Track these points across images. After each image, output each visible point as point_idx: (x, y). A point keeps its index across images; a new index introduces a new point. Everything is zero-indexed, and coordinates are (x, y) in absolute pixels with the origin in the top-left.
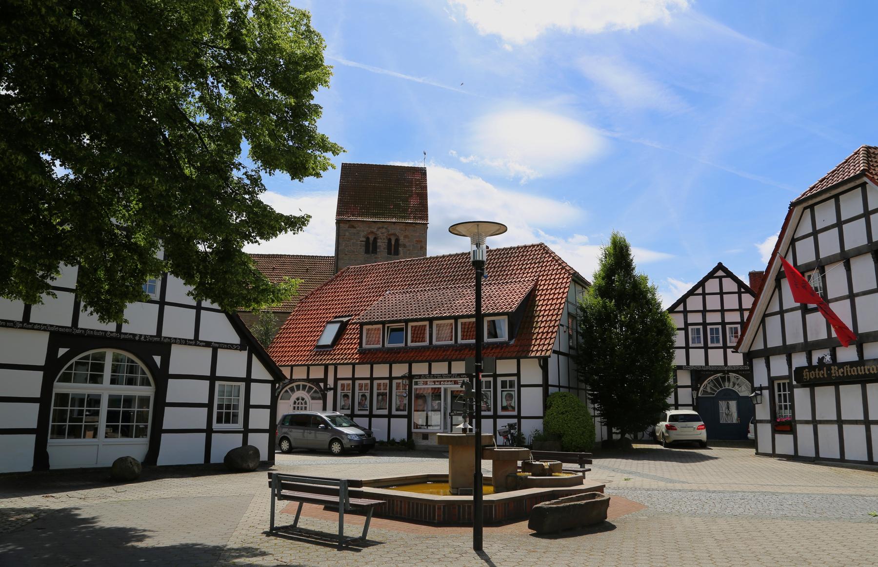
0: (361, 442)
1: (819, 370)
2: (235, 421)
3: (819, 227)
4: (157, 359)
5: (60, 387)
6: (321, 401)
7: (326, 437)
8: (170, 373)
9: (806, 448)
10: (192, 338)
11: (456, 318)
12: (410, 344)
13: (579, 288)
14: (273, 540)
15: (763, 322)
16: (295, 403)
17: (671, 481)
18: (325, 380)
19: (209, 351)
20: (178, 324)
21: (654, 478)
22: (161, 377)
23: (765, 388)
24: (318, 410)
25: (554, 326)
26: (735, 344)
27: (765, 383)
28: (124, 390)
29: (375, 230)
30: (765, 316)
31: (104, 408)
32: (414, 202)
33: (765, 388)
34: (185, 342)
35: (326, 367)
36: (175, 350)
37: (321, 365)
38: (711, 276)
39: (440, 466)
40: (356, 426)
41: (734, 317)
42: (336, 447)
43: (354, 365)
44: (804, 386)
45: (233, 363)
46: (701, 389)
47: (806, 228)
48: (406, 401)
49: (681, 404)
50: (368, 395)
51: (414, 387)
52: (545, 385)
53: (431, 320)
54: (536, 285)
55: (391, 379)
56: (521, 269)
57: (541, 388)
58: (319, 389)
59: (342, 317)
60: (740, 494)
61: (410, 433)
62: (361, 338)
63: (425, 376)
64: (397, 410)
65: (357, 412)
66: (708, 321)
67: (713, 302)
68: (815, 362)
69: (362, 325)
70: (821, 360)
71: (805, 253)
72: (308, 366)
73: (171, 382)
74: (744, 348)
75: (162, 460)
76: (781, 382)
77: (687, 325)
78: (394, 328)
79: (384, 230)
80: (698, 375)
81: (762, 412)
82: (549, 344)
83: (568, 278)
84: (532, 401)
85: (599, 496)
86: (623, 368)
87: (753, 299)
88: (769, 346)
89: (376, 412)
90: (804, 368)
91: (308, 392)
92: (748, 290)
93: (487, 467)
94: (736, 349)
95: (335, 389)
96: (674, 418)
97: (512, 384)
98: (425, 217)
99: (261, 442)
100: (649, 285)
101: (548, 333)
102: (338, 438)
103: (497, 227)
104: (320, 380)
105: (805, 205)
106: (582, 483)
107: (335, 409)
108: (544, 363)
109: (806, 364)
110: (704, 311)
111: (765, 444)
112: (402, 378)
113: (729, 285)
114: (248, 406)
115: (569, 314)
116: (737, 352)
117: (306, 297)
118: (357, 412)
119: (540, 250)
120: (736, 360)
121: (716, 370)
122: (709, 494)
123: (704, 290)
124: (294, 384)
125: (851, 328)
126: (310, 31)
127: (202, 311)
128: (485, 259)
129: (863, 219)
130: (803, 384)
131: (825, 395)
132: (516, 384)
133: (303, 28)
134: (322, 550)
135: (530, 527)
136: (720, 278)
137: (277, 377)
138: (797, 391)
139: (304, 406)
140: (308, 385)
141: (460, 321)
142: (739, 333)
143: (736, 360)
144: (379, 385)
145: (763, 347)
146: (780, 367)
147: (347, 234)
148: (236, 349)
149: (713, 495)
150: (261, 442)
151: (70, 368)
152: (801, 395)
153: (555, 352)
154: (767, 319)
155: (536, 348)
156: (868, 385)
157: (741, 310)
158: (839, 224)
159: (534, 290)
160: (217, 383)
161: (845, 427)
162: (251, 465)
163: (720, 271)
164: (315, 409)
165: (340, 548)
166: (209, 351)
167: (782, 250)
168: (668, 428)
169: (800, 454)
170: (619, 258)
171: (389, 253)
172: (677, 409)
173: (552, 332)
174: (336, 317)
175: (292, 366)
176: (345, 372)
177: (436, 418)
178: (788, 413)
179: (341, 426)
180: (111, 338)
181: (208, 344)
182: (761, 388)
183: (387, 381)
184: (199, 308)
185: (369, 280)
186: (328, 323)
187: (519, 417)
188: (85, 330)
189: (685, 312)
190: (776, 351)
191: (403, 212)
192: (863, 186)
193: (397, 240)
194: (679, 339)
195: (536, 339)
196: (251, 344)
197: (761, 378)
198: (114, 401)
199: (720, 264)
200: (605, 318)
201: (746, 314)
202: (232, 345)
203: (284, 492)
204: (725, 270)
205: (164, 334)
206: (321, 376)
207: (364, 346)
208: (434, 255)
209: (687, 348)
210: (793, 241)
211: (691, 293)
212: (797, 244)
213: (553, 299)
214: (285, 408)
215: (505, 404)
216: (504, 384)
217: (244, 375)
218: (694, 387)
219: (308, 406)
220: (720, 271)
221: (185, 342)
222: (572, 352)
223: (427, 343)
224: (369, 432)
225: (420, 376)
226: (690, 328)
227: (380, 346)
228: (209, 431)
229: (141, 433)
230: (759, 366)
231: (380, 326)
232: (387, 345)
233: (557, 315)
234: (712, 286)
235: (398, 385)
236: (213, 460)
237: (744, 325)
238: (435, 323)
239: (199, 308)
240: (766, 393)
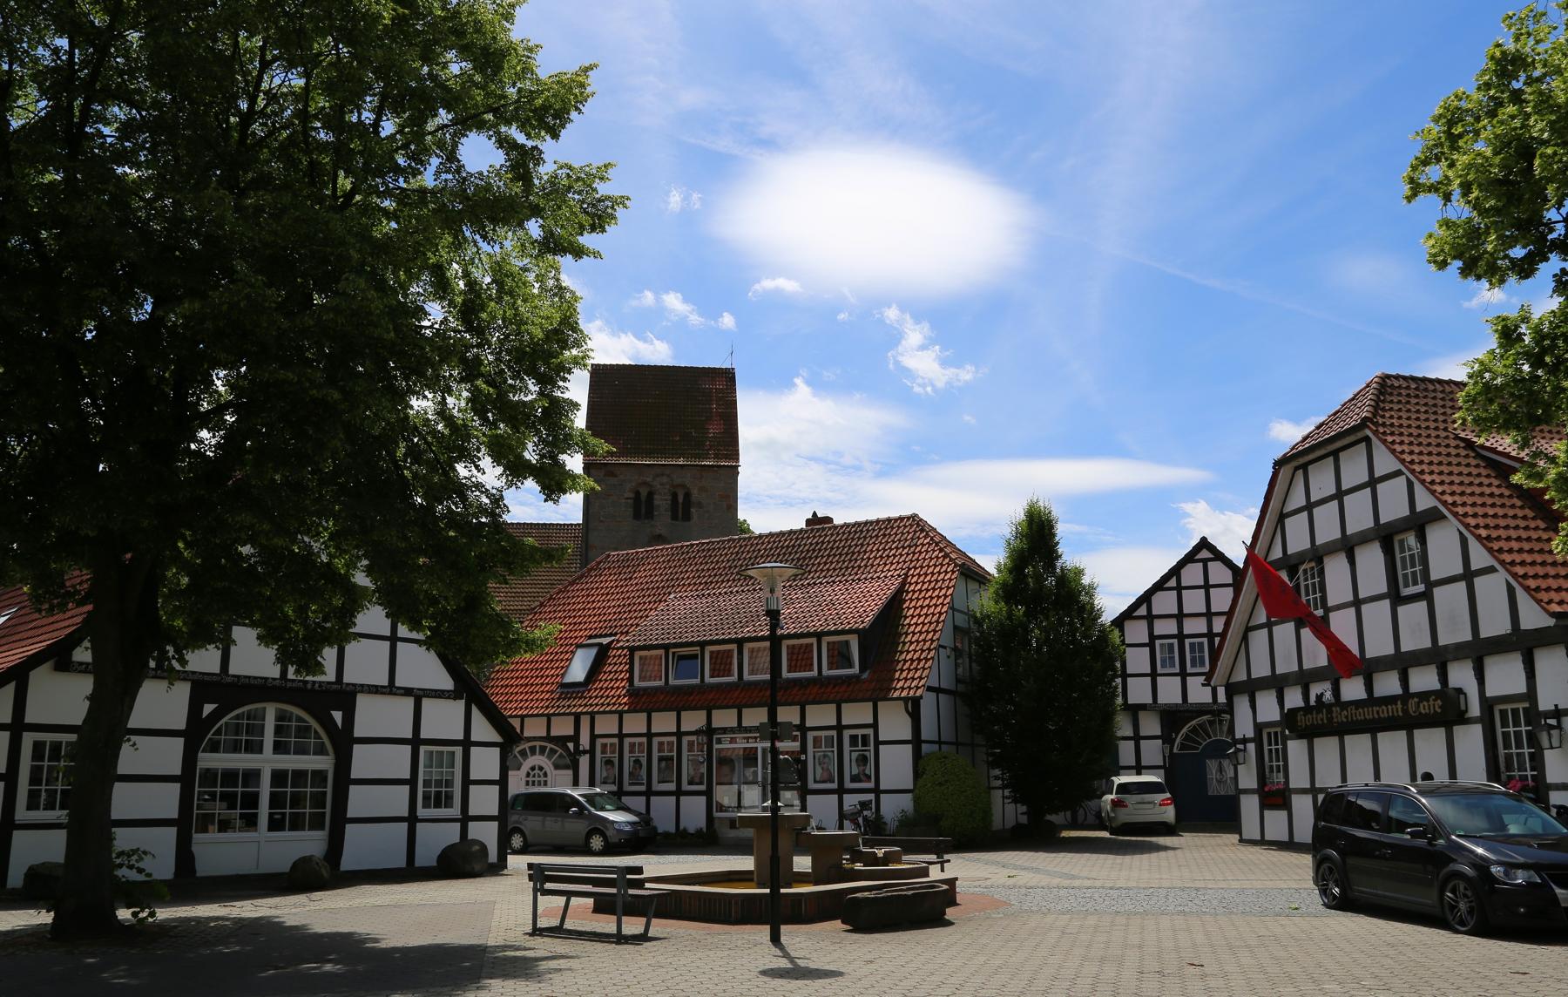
0: (634, 834)
2: (449, 804)
4: (338, 716)
5: (207, 760)
6: (570, 772)
7: (581, 827)
12: (708, 679)
13: (973, 586)
14: (539, 940)
15: (1245, 639)
17: (1073, 877)
18: (575, 738)
21: (1048, 873)
22: (344, 742)
23: (1250, 740)
24: (566, 786)
25: (929, 650)
27: (1250, 734)
28: (240, 761)
30: (1249, 629)
31: (265, 789)
32: (713, 430)
33: (1250, 740)
34: (375, 690)
35: (577, 717)
36: (363, 702)
38: (1189, 558)
39: (746, 863)
40: (626, 809)
42: (597, 843)
43: (621, 714)
44: (1300, 737)
45: (445, 719)
47: (1297, 499)
48: (704, 770)
49: (1139, 771)
50: (644, 761)
51: (716, 746)
52: (916, 741)
53: (740, 642)
54: (903, 584)
57: (910, 747)
58: (567, 753)
59: (601, 636)
62: (631, 671)
63: (732, 730)
64: (690, 783)
66: (808, 724)
69: (632, 650)
70: (1319, 697)
71: (1297, 538)
72: (549, 716)
75: (348, 863)
76: (1272, 730)
78: (683, 654)
79: (665, 479)
80: (1172, 718)
82: (921, 678)
84: (896, 766)
86: (1033, 710)
89: (657, 787)
90: (1299, 709)
91: (549, 757)
95: (592, 752)
96: (1123, 788)
98: (735, 455)
99: (487, 834)
100: (1086, 581)
101: (919, 660)
102: (600, 827)
106: (927, 875)
107: (592, 784)
108: (913, 708)
111: (1250, 826)
113: (1218, 573)
114: (467, 782)
115: (955, 628)
117: (542, 605)
118: (627, 788)
121: (1200, 710)
124: (527, 746)
125: (1355, 651)
126: (561, 288)
130: (1301, 734)
132: (869, 742)
133: (551, 283)
134: (599, 946)
136: (1205, 562)
137: (509, 740)
138: (1291, 744)
140: (549, 746)
144: (661, 744)
145: (1469, 637)
146: (1268, 709)
150: (487, 834)
151: (218, 732)
152: (1296, 749)
153: (930, 689)
154: (1251, 634)
155: (900, 684)
156: (1455, 728)
159: (901, 590)
160: (422, 749)
162: (477, 867)
164: (560, 784)
165: (618, 943)
166: (410, 701)
168: (1116, 804)
170: (1037, 534)
171: (674, 517)
172: (1139, 773)
173: (927, 660)
174: (590, 637)
175: (523, 717)
176: (606, 725)
177: (752, 795)
179: (603, 809)
180: (274, 687)
181: (408, 692)
182: (1245, 741)
184: (393, 639)
185: (641, 575)
186: (579, 646)
187: (877, 791)
188: (238, 677)
189: (1150, 618)
190: (1499, 646)
191: (695, 447)
193: (687, 495)
194: (1137, 660)
195: (902, 670)
196: (469, 691)
198: (279, 777)
199: (1204, 539)
200: (1010, 635)
201: (1218, 625)
202: (443, 691)
203: (548, 886)
204: (1212, 548)
205: (346, 680)
207: (637, 683)
209: (1154, 675)
210: (1282, 517)
211: (1159, 586)
212: (1287, 521)
213: (929, 606)
214: (517, 785)
215: (855, 771)
216: (854, 739)
218: (1167, 738)
219: (549, 779)
220: (1204, 551)
221: (375, 690)
222: (961, 688)
223: (734, 678)
224: (645, 819)
225: (724, 730)
226: (1158, 642)
227: (662, 683)
228: (412, 820)
229: (317, 824)
231: (662, 652)
232: (672, 682)
233: (935, 631)
234: (1192, 575)
235: (691, 744)
236: (419, 863)
238: (747, 646)
239: (393, 639)
240: (1251, 747)
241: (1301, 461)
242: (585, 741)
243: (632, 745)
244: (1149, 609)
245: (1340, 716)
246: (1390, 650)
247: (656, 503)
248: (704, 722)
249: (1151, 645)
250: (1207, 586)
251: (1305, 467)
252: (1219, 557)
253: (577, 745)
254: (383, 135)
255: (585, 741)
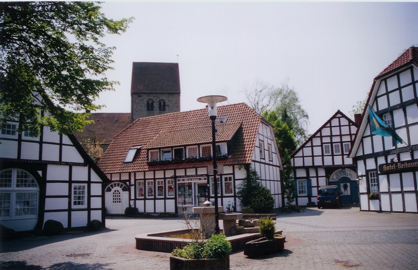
1: (391, 165)
3: (389, 90)
4: (40, 173)
8: (47, 180)
9: (386, 207)
10: (58, 161)
11: (199, 145)
15: (362, 141)
16: (114, 193)
18: (129, 180)
19: (67, 168)
20: (50, 153)
22: (43, 182)
26: (348, 153)
29: (152, 98)
30: (363, 137)
37: (127, 172)
38: (334, 117)
39: (195, 224)
41: (347, 139)
45: (81, 173)
46: (331, 177)
47: (383, 91)
51: (178, 182)
54: (241, 125)
55: (165, 178)
56: (233, 117)
59: (137, 146)
60: (352, 232)
61: (176, 208)
63: (183, 177)
65: (147, 197)
66: (333, 141)
67: (336, 131)
68: (389, 161)
69: (148, 150)
70: (392, 160)
71: (383, 104)
72: (120, 173)
73: (48, 184)
74: (352, 155)
76: (372, 172)
77: (322, 143)
81: (363, 188)
83: (258, 121)
85: (280, 236)
87: (356, 129)
88: (365, 154)
90: (384, 164)
91: (121, 187)
92: (354, 124)
93: (221, 223)
94: (348, 155)
95: (135, 185)
97: (230, 179)
103: (222, 98)
104: (127, 181)
105: (382, 78)
109: (385, 163)
110: (331, 136)
112: (171, 178)
113: (344, 122)
116: (349, 157)
119: (243, 106)
120: (349, 161)
121: (338, 167)
122: (336, 233)
123: (331, 124)
124: (113, 183)
127: (63, 146)
128: (216, 115)
129: (412, 86)
130: (382, 174)
131: (395, 178)
135: (245, 254)
136: (339, 118)
137: (106, 183)
138: (380, 177)
139: (119, 195)
140: (121, 183)
141: (201, 146)
142: (350, 147)
143: (349, 161)
144: (158, 182)
146: (371, 165)
147: (137, 100)
148: (82, 166)
149: (338, 233)
152: (383, 180)
153: (253, 161)
154: (364, 139)
157: (351, 135)
158: (400, 88)
161: (59, 142)
163: (339, 115)
166: (67, 168)
167: (370, 103)
169: (383, 210)
171: (160, 110)
174: (134, 146)
175: (111, 174)
176: (140, 176)
178: (376, 188)
181: (66, 164)
183: (163, 180)
184: (61, 144)
190: (369, 156)
192: (412, 68)
193: (164, 103)
197: (361, 171)
201: (353, 137)
202: (80, 163)
204: (341, 113)
206: (127, 178)
208: (185, 111)
209: (323, 156)
210: (376, 98)
211: (324, 126)
216: (226, 179)
217: (87, 180)
219: (121, 195)
220: (339, 115)
225: (180, 177)
226: (324, 145)
230: (360, 164)
231: (158, 150)
234: (335, 122)
237: (352, 143)
240: (364, 178)
241: (385, 77)
242: (133, 182)
243: (149, 183)
244: (321, 134)
245: (400, 166)
246: (382, 150)
247: (154, 105)
248: (174, 174)
249: (322, 146)
250: (340, 126)
251: (385, 80)
252: (344, 116)
253: (130, 183)
254: (74, 25)
255: (133, 182)
